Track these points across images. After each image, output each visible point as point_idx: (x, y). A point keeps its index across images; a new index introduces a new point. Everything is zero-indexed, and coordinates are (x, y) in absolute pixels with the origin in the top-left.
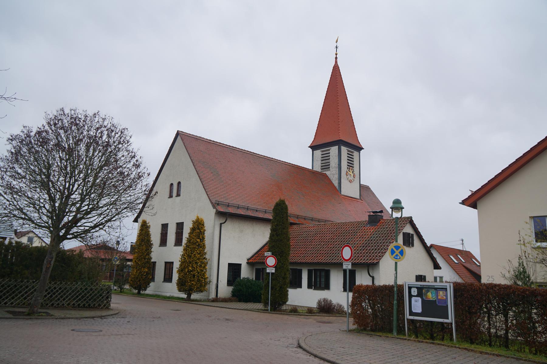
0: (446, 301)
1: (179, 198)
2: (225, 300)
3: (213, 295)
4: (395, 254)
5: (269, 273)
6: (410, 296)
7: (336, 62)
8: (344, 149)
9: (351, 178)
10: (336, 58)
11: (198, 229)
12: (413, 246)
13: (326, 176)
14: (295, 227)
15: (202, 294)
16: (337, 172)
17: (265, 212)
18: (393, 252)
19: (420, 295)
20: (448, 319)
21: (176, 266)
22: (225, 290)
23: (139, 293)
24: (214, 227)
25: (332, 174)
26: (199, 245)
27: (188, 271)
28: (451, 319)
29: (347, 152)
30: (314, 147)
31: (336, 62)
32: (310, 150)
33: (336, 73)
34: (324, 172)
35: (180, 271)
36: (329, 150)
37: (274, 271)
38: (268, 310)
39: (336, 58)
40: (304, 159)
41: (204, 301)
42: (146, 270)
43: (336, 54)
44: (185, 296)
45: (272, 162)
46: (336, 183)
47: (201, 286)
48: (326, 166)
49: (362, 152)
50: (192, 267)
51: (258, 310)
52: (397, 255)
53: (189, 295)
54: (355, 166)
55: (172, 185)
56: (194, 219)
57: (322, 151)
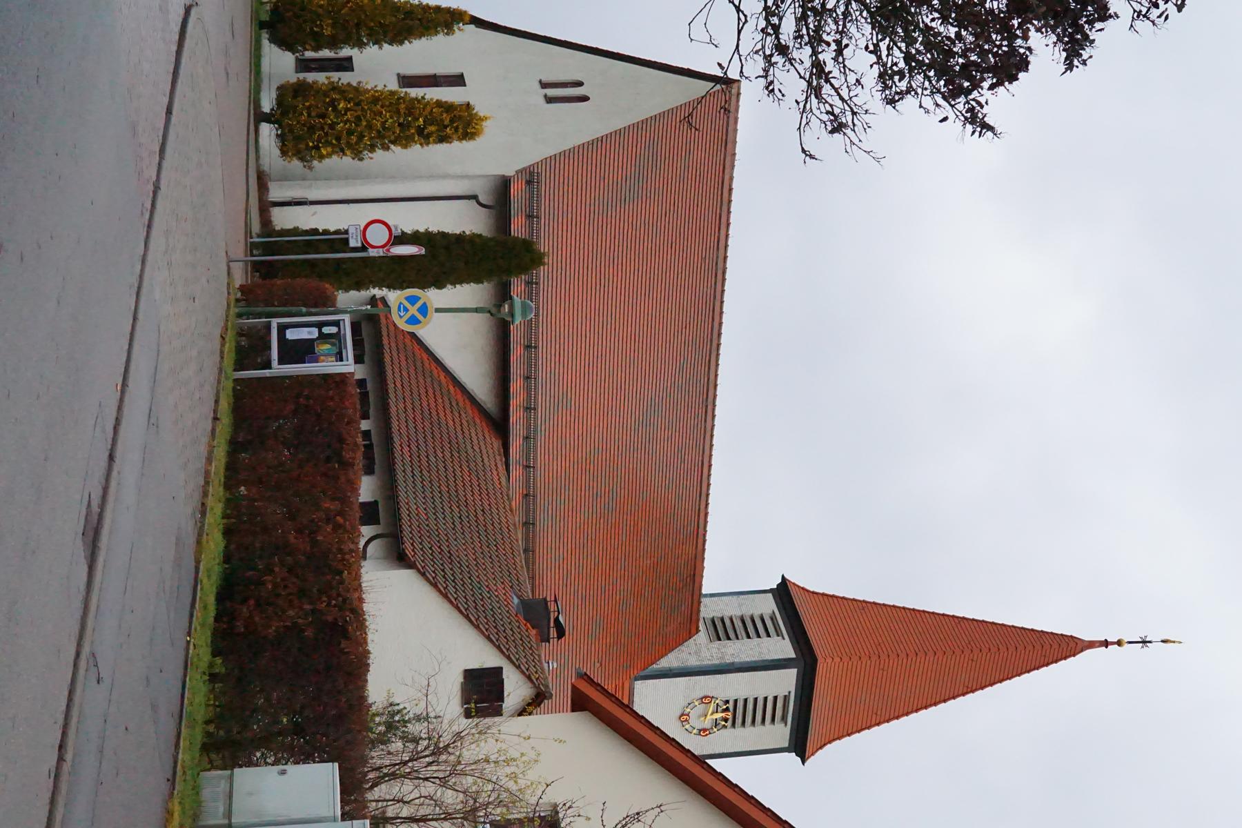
1: (542, 100)
2: (266, 222)
3: (276, 192)
4: (407, 305)
6: (319, 325)
7: (1091, 645)
8: (785, 682)
9: (696, 722)
10: (1106, 644)
11: (452, 121)
13: (690, 629)
14: (497, 444)
18: (413, 321)
21: (345, 78)
23: (260, 117)
25: (700, 649)
26: (409, 125)
28: (278, 369)
29: (781, 693)
30: (784, 592)
31: (1091, 645)
32: (774, 583)
33: (1063, 647)
34: (701, 626)
35: (334, 88)
36: (779, 633)
39: (1106, 644)
40: (738, 560)
42: (328, 31)
43: (1119, 643)
44: (267, 105)
46: (671, 661)
47: (298, 139)
48: (722, 630)
50: (347, 110)
51: (247, 225)
52: (406, 310)
53: (267, 118)
54: (739, 730)
55: (580, 84)
56: (480, 109)
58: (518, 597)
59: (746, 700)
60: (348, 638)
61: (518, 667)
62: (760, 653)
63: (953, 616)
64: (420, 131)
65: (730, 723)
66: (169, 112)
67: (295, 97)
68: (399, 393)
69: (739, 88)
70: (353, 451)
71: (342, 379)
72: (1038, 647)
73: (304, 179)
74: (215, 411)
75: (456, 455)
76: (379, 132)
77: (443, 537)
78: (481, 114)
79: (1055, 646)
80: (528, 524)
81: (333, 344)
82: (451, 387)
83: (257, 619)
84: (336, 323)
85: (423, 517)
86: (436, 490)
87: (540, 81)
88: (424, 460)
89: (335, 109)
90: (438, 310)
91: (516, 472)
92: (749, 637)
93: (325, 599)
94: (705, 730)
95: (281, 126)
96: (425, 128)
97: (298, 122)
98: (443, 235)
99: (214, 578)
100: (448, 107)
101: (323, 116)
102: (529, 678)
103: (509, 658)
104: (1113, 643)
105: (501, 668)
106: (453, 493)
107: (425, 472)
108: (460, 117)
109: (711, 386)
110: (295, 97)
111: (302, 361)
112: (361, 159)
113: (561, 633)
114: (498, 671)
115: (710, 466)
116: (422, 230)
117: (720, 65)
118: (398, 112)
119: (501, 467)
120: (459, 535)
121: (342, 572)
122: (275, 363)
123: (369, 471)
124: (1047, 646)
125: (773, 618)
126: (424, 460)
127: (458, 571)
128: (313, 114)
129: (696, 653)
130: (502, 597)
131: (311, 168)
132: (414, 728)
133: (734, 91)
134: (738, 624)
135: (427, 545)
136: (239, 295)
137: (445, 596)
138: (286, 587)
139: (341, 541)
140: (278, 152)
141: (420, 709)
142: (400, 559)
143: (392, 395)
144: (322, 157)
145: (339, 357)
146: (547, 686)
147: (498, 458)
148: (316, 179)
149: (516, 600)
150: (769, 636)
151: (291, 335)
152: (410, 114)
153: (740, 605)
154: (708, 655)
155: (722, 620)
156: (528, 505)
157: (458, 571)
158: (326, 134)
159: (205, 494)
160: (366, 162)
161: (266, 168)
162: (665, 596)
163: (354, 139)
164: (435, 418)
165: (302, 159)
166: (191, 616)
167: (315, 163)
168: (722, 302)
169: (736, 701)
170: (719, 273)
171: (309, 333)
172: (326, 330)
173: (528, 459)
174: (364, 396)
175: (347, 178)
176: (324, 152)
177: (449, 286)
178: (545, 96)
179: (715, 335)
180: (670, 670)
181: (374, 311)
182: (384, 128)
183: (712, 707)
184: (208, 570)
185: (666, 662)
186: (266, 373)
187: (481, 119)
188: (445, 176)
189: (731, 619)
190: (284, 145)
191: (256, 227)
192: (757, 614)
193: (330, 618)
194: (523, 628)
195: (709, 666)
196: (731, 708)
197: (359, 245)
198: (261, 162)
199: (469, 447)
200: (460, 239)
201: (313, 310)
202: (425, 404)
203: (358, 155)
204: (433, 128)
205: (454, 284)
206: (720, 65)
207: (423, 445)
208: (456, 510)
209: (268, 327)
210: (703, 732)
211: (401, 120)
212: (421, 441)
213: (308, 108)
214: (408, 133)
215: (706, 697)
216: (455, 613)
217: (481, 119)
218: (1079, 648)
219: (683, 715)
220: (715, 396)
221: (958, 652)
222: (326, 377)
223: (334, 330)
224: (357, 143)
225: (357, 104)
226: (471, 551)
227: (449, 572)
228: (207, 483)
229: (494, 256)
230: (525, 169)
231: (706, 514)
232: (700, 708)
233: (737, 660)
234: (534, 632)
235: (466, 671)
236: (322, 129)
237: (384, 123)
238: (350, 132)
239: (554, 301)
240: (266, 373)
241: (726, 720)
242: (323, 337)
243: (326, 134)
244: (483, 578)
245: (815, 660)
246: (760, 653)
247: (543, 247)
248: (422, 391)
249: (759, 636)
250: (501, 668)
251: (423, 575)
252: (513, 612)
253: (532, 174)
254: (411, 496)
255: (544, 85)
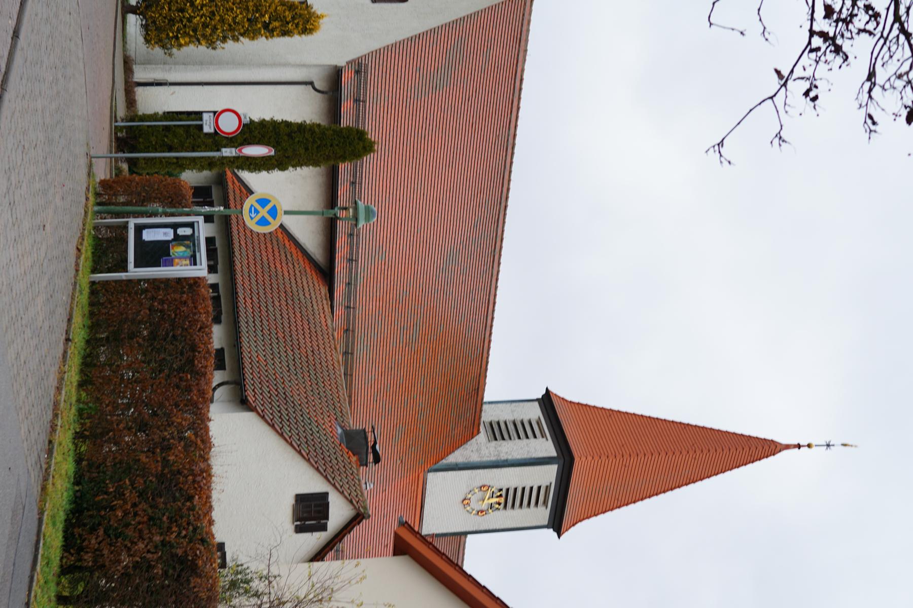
0: (171, 263)
2: (131, 102)
5: (201, 119)
6: (175, 226)
7: (788, 447)
8: (548, 475)
10: (799, 446)
11: (293, 18)
12: (299, 530)
13: (473, 432)
14: (324, 290)
15: (141, 40)
16: (485, 459)
20: (135, 267)
22: (155, 102)
24: (304, 66)
25: (480, 447)
28: (134, 272)
30: (547, 401)
31: (788, 447)
33: (766, 448)
36: (543, 435)
38: (116, 121)
39: (799, 446)
40: (511, 379)
41: (124, 46)
43: (809, 446)
45: (490, 259)
46: (456, 457)
48: (498, 432)
49: (551, 533)
52: (257, 212)
53: (134, 10)
54: (509, 512)
57: (539, 423)
58: (342, 427)
60: (200, 577)
61: (342, 493)
64: (266, 26)
65: (502, 506)
66: (16, 34)
71: (195, 282)
73: (164, 64)
74: (67, 332)
76: (230, 25)
77: (280, 381)
78: (319, 13)
79: (760, 448)
81: (187, 247)
82: (286, 242)
83: (106, 552)
84: (191, 225)
85: (263, 363)
86: (274, 336)
90: (286, 213)
91: (339, 311)
93: (175, 529)
94: (482, 512)
95: (145, 17)
97: (161, 15)
98: (287, 124)
99: (60, 526)
101: (182, 10)
102: (351, 502)
103: (334, 485)
106: (288, 339)
107: (265, 322)
111: (158, 265)
112: (214, 48)
113: (377, 459)
114: (325, 495)
115: (494, 303)
116: (268, 118)
117: (778, 72)
118: (247, 9)
120: (293, 377)
121: (193, 497)
123: (217, 320)
124: (753, 448)
125: (539, 423)
126: (264, 309)
127: (291, 410)
128: (173, 8)
129: (477, 450)
130: (329, 430)
131: (170, 55)
132: (256, 585)
135: (266, 390)
136: (99, 189)
137: (281, 435)
139: (192, 462)
141: (262, 568)
142: (243, 403)
143: (237, 254)
144: (180, 46)
145: (194, 261)
146: (365, 508)
147: (325, 302)
148: (176, 64)
149: (340, 431)
151: (149, 235)
153: (512, 411)
154: (487, 452)
155: (498, 423)
156: (348, 338)
157: (291, 410)
158: (185, 26)
159: (53, 428)
162: (454, 408)
163: (208, 31)
164: (273, 270)
165: (163, 47)
166: (31, 578)
167: (175, 50)
168: (510, 172)
169: (508, 490)
171: (165, 234)
172: (181, 231)
173: (349, 301)
174: (217, 299)
175: (201, 63)
176: (182, 42)
177: (291, 169)
179: (504, 199)
180: (457, 465)
181: (228, 212)
182: (235, 23)
183: (489, 494)
184: (53, 517)
187: (318, 17)
188: (286, 65)
189: (506, 423)
190: (147, 34)
191: (121, 112)
193: (180, 552)
194: (346, 456)
195: (487, 462)
196: (504, 495)
197: (212, 131)
198: (128, 46)
199: (301, 295)
200: (301, 128)
201: (169, 210)
202: (265, 259)
203: (211, 44)
204: (276, 24)
205: (294, 166)
206: (778, 72)
207: (263, 296)
208: (290, 353)
209: (125, 227)
211: (250, 16)
212: (261, 294)
214: (255, 27)
215: (484, 486)
216: (289, 449)
218: (778, 449)
219: (465, 499)
221: (684, 453)
222: (179, 281)
223: (187, 231)
226: (302, 390)
227: (284, 412)
228: (56, 416)
230: (354, 61)
231: (490, 341)
232: (479, 494)
233: (510, 457)
234: (354, 459)
236: (181, 21)
237: (234, 19)
238: (205, 25)
241: (499, 504)
242: (177, 238)
243: (185, 26)
244: (313, 414)
246: (528, 452)
247: (372, 136)
248: (263, 247)
251: (263, 417)
252: (337, 442)
253: (360, 65)
254: (253, 344)
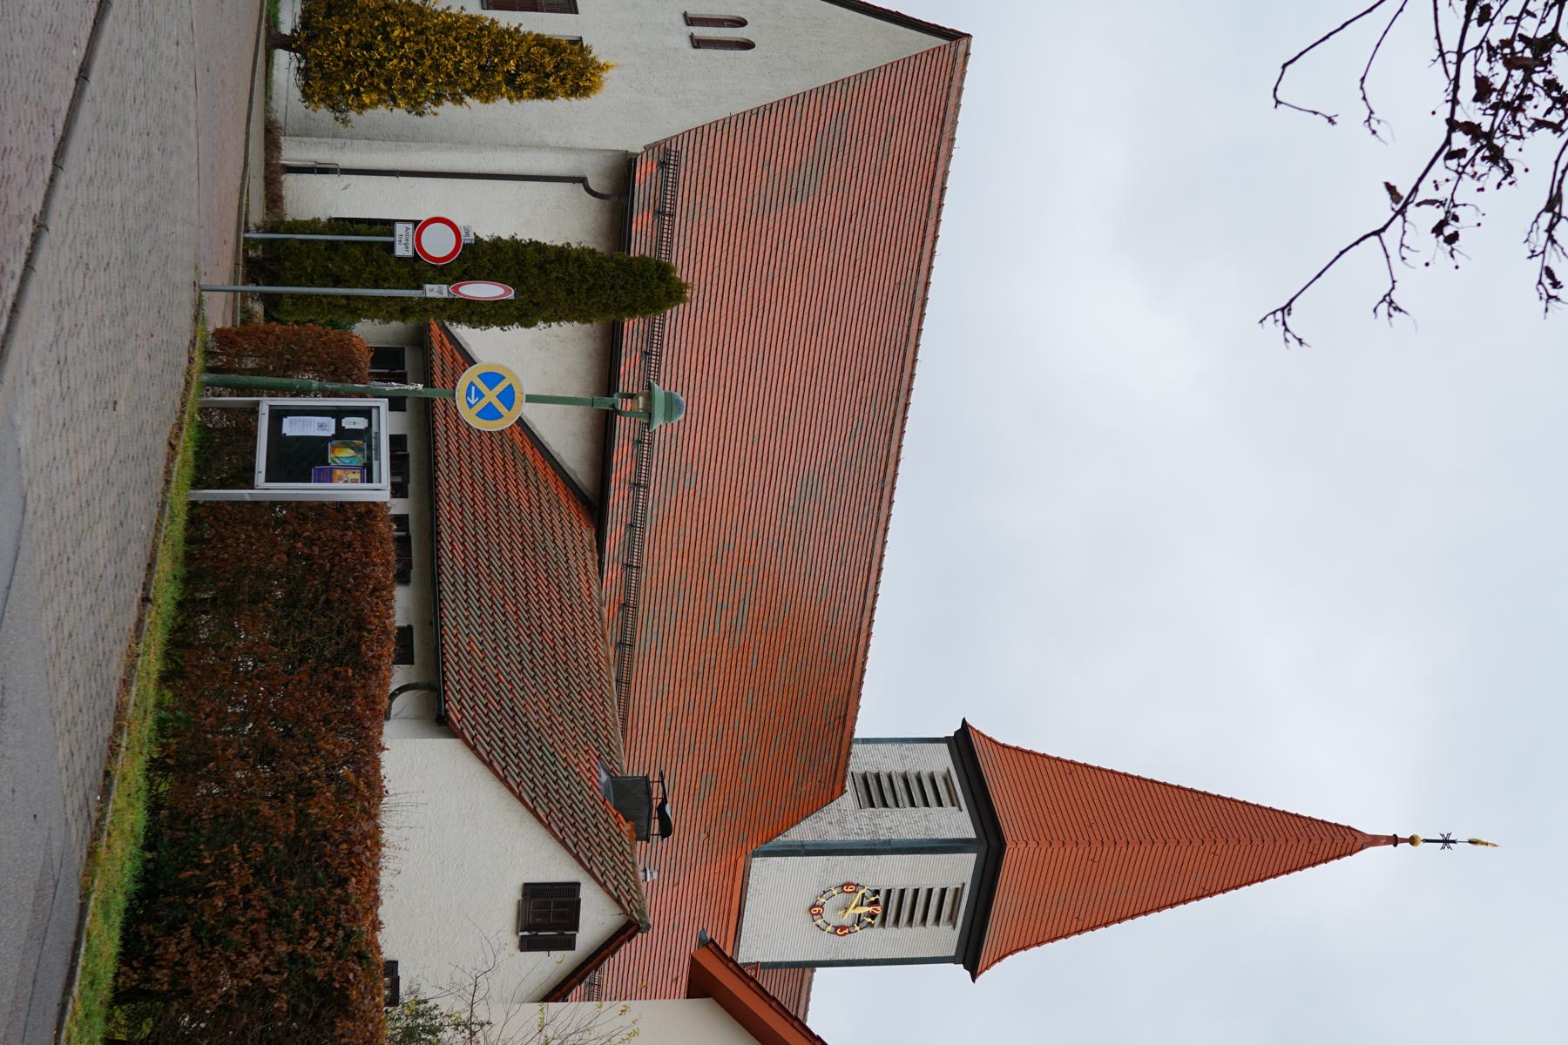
1: (687, 44)
2: (274, 199)
5: (392, 234)
6: (338, 414)
7: (1376, 841)
8: (959, 870)
9: (832, 916)
10: (1395, 840)
11: (557, 68)
12: (527, 945)
13: (833, 791)
14: (589, 535)
15: (297, 94)
17: (639, 442)
19: (342, 434)
23: (276, 41)
24: (571, 149)
25: (844, 817)
27: (385, 24)
28: (265, 489)
29: (952, 886)
30: (963, 743)
31: (1376, 841)
33: (1337, 842)
36: (954, 802)
37: (400, 251)
39: (1395, 840)
40: (902, 701)
43: (1412, 841)
44: (286, 29)
46: (802, 832)
48: (876, 792)
49: (960, 971)
50: (404, 40)
52: (480, 395)
53: (286, 43)
55: (741, 23)
56: (599, 53)
58: (608, 772)
59: (902, 892)
61: (603, 885)
62: (927, 829)
63: (1191, 790)
64: (510, 79)
65: (878, 920)
66: (83, 74)
67: (328, 16)
68: (454, 462)
69: (968, 47)
70: (381, 643)
71: (368, 512)
72: (1304, 840)
73: (334, 136)
74: (146, 587)
75: (529, 552)
76: (448, 75)
78: (601, 61)
80: (624, 645)
81: (358, 449)
83: (192, 968)
84: (366, 413)
87: (685, 15)
88: (483, 562)
89: (386, 37)
91: (612, 572)
92: (913, 804)
94: (843, 928)
95: (304, 56)
96: (517, 74)
97: (332, 53)
98: (537, 247)
100: (552, 46)
101: (369, 47)
102: (618, 901)
103: (590, 871)
104: (1404, 840)
105: (578, 884)
107: (485, 585)
108: (570, 63)
109: (892, 460)
110: (328, 16)
112: (420, 114)
113: (666, 830)
114: (573, 888)
116: (505, 236)
117: (1391, 189)
119: (592, 568)
121: (347, 880)
122: (260, 477)
123: (403, 578)
125: (947, 779)
126: (483, 562)
131: (345, 122)
133: (962, 48)
134: (899, 785)
135: (481, 701)
136: (212, 345)
138: (247, 905)
140: (297, 94)
141: (459, 1007)
142: (440, 722)
144: (363, 107)
145: (368, 474)
146: (642, 912)
147: (589, 555)
148: (352, 138)
149: (604, 777)
150: (940, 804)
151: (291, 427)
152: (497, 53)
153: (903, 758)
154: (855, 825)
155: (877, 777)
157: (522, 738)
160: (427, 119)
161: (279, 116)
162: (802, 747)
163: (412, 83)
164: (503, 496)
165: (333, 108)
167: (352, 114)
169: (889, 892)
170: (918, 304)
172: (349, 423)
177: (541, 324)
178: (692, 37)
179: (903, 392)
182: (457, 72)
184: (106, 903)
185: (796, 834)
186: (245, 494)
187: (601, 68)
188: (542, 147)
189: (890, 777)
190: (307, 84)
191: (257, 215)
192: (925, 772)
193: (319, 974)
197: (410, 253)
198: (273, 105)
200: (562, 255)
203: (416, 107)
204: (528, 77)
206: (1391, 189)
207: (483, 540)
209: (254, 411)
210: (840, 929)
213: (347, 34)
214: (491, 81)
215: (848, 884)
217: (601, 68)
219: (814, 906)
220: (895, 475)
222: (341, 507)
223: (360, 423)
224: (415, 91)
225: (418, 33)
227: (510, 741)
229: (605, 285)
231: (869, 635)
233: (895, 837)
234: (627, 827)
235: (526, 885)
236: (366, 65)
238: (407, 74)
239: (685, 348)
240: (245, 494)
241: (873, 916)
242: (342, 434)
243: (372, 74)
245: (1002, 845)
246: (927, 829)
249: (927, 804)
250: (578, 884)
251: (473, 748)
253: (667, 152)
255: (691, 21)
